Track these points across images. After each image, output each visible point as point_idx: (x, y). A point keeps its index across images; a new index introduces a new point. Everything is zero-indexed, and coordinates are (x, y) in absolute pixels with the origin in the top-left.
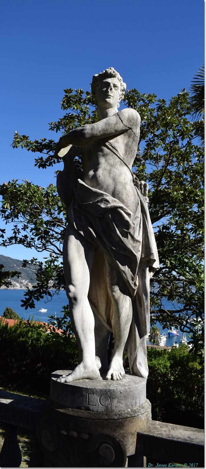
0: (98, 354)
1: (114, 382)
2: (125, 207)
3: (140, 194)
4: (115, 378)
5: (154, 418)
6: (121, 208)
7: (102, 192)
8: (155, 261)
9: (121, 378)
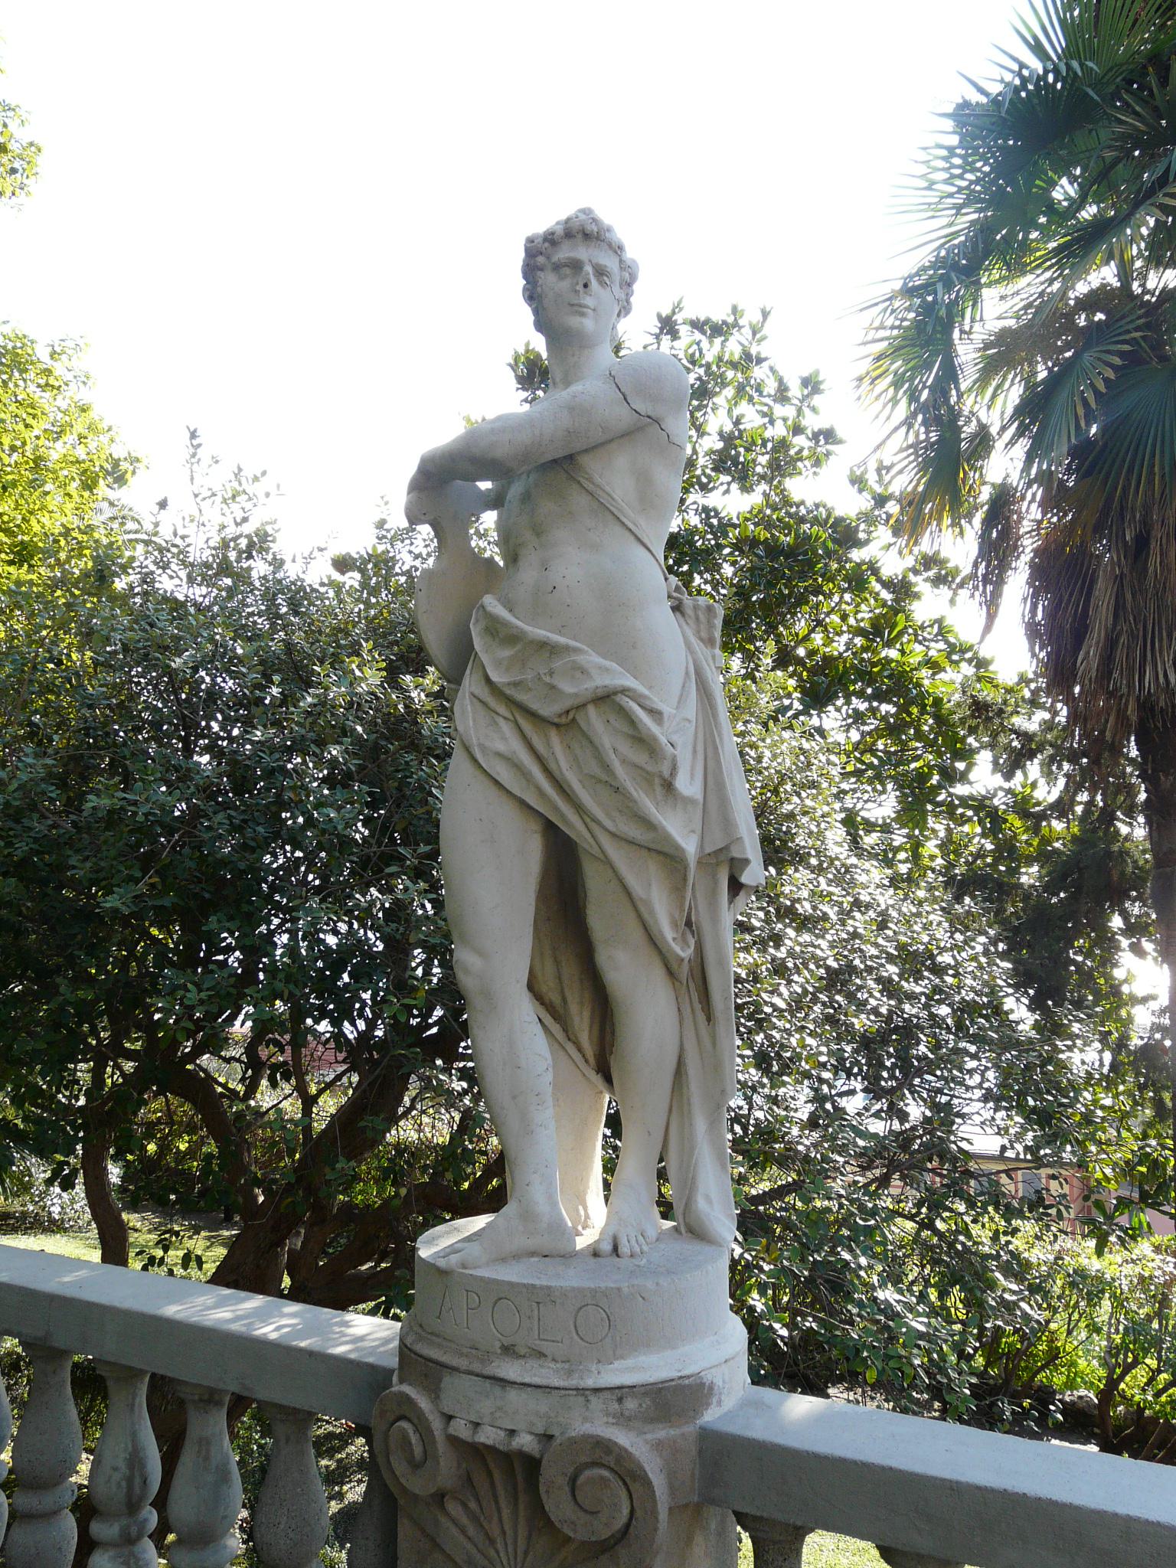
0: (983, 524)
1: (623, 1262)
2: (642, 689)
3: (693, 640)
4: (624, 1249)
5: (757, 1380)
6: (624, 691)
7: (562, 640)
8: (746, 862)
9: (645, 1248)
